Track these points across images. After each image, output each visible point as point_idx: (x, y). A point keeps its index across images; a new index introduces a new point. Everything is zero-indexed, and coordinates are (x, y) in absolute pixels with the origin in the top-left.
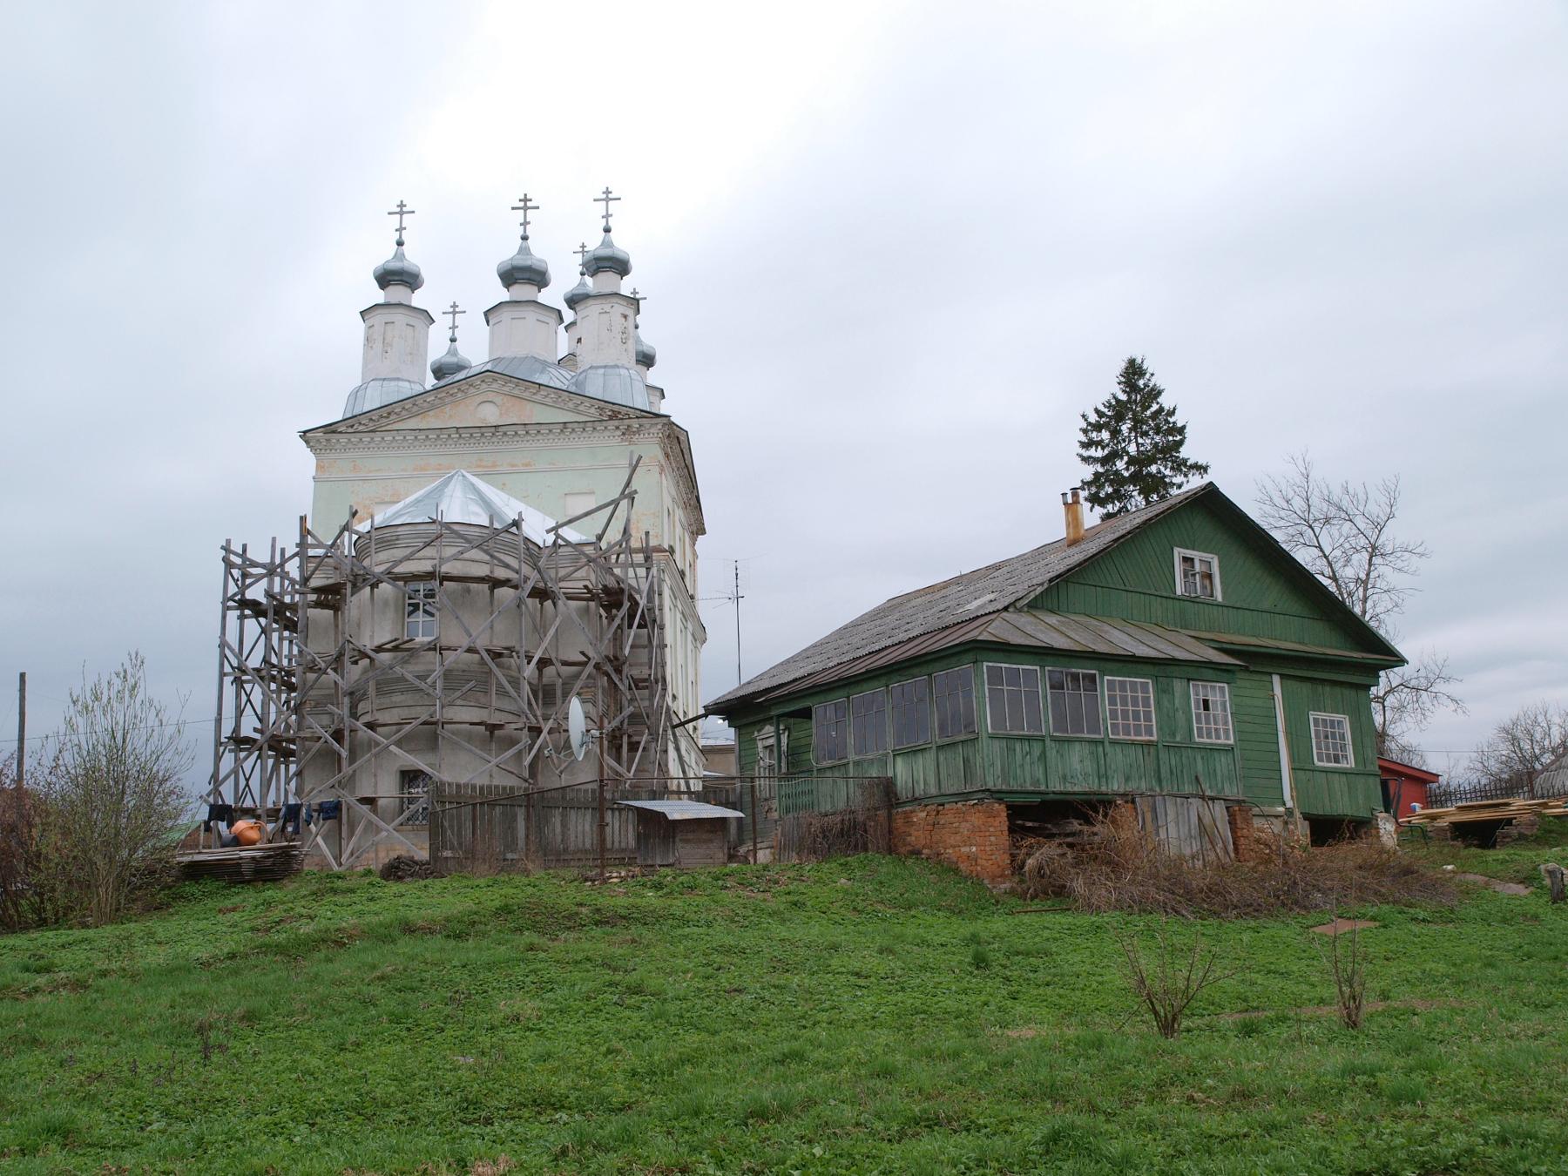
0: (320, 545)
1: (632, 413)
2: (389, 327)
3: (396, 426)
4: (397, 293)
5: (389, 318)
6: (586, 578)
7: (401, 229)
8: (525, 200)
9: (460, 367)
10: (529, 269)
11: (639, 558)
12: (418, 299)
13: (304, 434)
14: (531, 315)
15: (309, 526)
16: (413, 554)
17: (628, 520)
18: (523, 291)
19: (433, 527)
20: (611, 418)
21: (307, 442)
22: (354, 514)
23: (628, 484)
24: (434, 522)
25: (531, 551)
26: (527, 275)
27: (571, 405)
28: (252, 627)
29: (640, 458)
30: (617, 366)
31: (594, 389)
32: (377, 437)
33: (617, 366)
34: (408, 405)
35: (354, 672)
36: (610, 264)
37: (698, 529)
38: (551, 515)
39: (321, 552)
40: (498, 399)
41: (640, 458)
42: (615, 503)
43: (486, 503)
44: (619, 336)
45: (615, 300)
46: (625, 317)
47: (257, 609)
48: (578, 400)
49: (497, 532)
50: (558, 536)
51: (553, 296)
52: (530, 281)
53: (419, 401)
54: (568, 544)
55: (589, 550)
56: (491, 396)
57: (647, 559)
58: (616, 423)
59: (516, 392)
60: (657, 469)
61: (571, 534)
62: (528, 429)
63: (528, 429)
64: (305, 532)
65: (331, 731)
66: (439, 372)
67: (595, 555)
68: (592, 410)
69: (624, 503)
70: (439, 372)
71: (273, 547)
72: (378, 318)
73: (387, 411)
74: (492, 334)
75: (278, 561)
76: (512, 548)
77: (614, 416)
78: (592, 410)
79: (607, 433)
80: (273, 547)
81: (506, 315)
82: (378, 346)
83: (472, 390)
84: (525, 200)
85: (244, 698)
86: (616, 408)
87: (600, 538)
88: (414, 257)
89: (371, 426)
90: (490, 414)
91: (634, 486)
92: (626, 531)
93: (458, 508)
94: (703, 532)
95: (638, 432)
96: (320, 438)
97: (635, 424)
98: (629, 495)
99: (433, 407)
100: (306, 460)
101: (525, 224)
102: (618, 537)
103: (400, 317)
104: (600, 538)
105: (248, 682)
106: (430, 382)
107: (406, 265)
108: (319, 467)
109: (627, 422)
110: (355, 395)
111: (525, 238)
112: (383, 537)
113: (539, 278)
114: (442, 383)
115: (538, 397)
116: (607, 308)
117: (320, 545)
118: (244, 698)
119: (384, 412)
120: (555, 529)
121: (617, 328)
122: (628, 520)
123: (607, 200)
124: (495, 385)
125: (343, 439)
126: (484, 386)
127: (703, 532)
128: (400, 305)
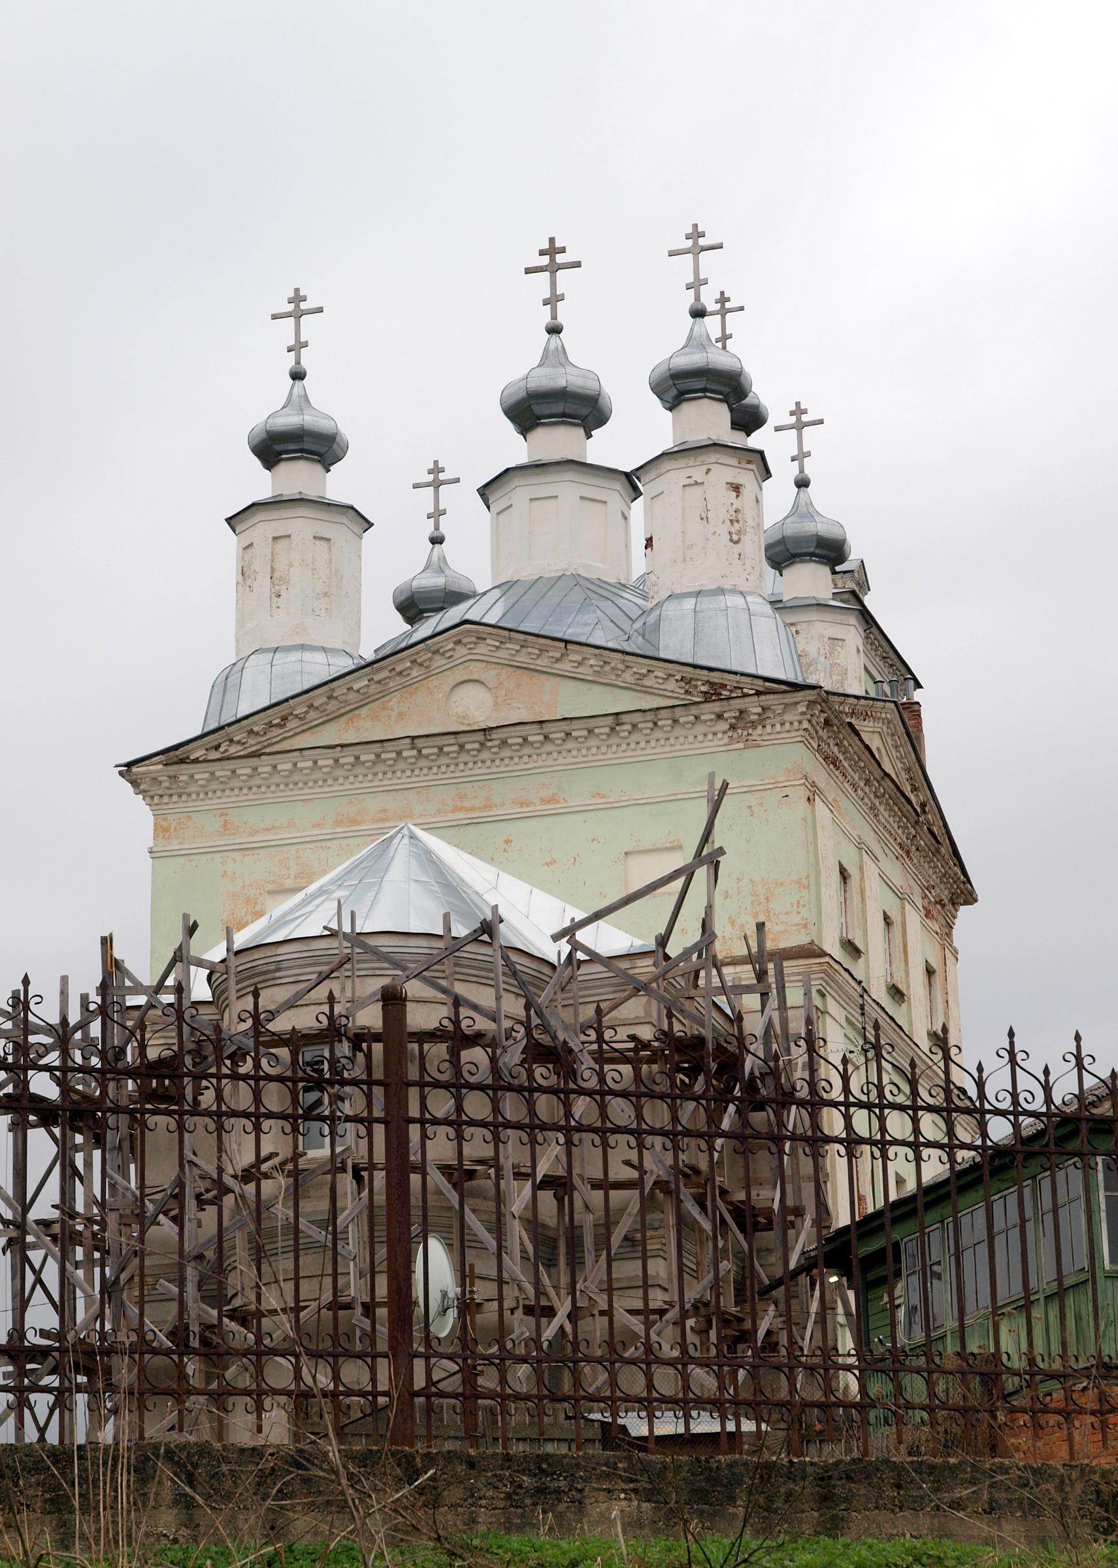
0: (138, 989)
1: (749, 687)
2: (282, 543)
3: (286, 745)
4: (297, 477)
5: (280, 528)
6: (636, 1019)
7: (297, 347)
8: (552, 250)
9: (452, 597)
10: (561, 395)
11: (746, 973)
12: (337, 484)
13: (128, 769)
14: (568, 488)
15: (117, 954)
16: (298, 996)
17: (709, 908)
18: (555, 441)
19: (333, 943)
20: (707, 698)
21: (135, 783)
22: (191, 929)
23: (706, 837)
24: (333, 934)
25: (523, 972)
26: (559, 408)
27: (628, 677)
28: (42, 1145)
29: (725, 785)
30: (721, 591)
31: (675, 643)
32: (264, 765)
33: (721, 591)
34: (319, 698)
35: (203, 1224)
36: (707, 384)
37: (951, 888)
38: (568, 897)
39: (141, 1000)
40: (490, 675)
41: (725, 785)
42: (687, 873)
43: (447, 884)
44: (724, 529)
45: (713, 457)
46: (737, 488)
47: (47, 1114)
48: (641, 666)
49: (457, 944)
50: (576, 946)
51: (614, 446)
52: (565, 418)
53: (340, 689)
54: (594, 958)
55: (645, 969)
56: (477, 671)
57: (761, 975)
58: (716, 707)
59: (522, 658)
60: (803, 793)
61: (608, 939)
62: (547, 731)
63: (547, 731)
64: (112, 968)
65: (167, 1328)
66: (412, 607)
67: (667, 973)
68: (671, 685)
69: (702, 873)
70: (412, 607)
71: (64, 994)
72: (262, 529)
73: (281, 713)
74: (496, 530)
75: (74, 1017)
76: (482, 974)
77: (714, 693)
78: (671, 685)
79: (700, 729)
80: (64, 994)
81: (520, 493)
82: (263, 584)
83: (439, 661)
84: (552, 250)
85: (30, 1278)
86: (715, 677)
87: (663, 941)
88: (329, 405)
89: (253, 744)
90: (474, 706)
91: (719, 839)
92: (706, 926)
93: (400, 906)
94: (970, 898)
95: (761, 721)
96: (162, 773)
97: (753, 707)
98: (708, 857)
99: (366, 700)
100: (136, 814)
101: (553, 300)
102: (695, 936)
103: (300, 525)
104: (663, 941)
105: (34, 1246)
106: (395, 627)
107: (308, 420)
108: (160, 830)
109: (737, 704)
110: (227, 683)
111: (554, 330)
112: (247, 970)
113: (587, 411)
114: (426, 629)
115: (565, 666)
116: (698, 474)
117: (138, 989)
118: (30, 1278)
119: (274, 716)
120: (568, 933)
121: (720, 515)
122: (709, 908)
123: (697, 250)
124: (481, 649)
125: (201, 773)
126: (461, 651)
127: (970, 898)
128: (300, 501)
